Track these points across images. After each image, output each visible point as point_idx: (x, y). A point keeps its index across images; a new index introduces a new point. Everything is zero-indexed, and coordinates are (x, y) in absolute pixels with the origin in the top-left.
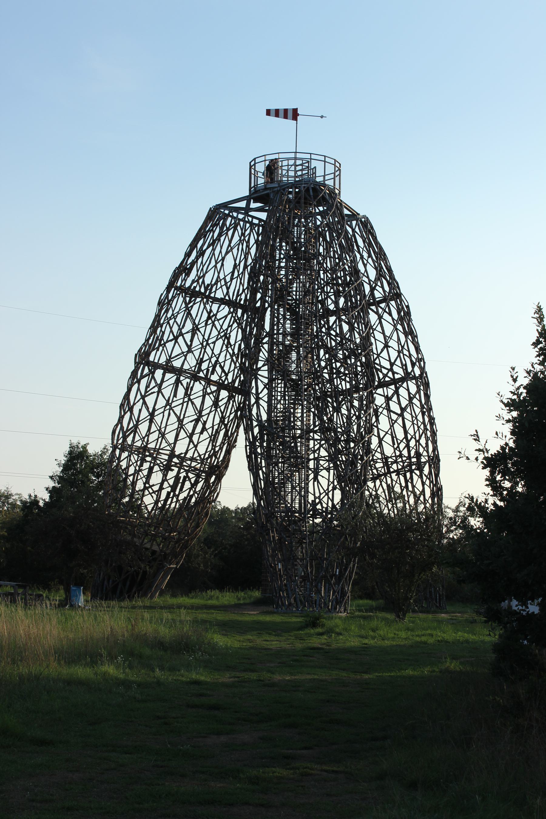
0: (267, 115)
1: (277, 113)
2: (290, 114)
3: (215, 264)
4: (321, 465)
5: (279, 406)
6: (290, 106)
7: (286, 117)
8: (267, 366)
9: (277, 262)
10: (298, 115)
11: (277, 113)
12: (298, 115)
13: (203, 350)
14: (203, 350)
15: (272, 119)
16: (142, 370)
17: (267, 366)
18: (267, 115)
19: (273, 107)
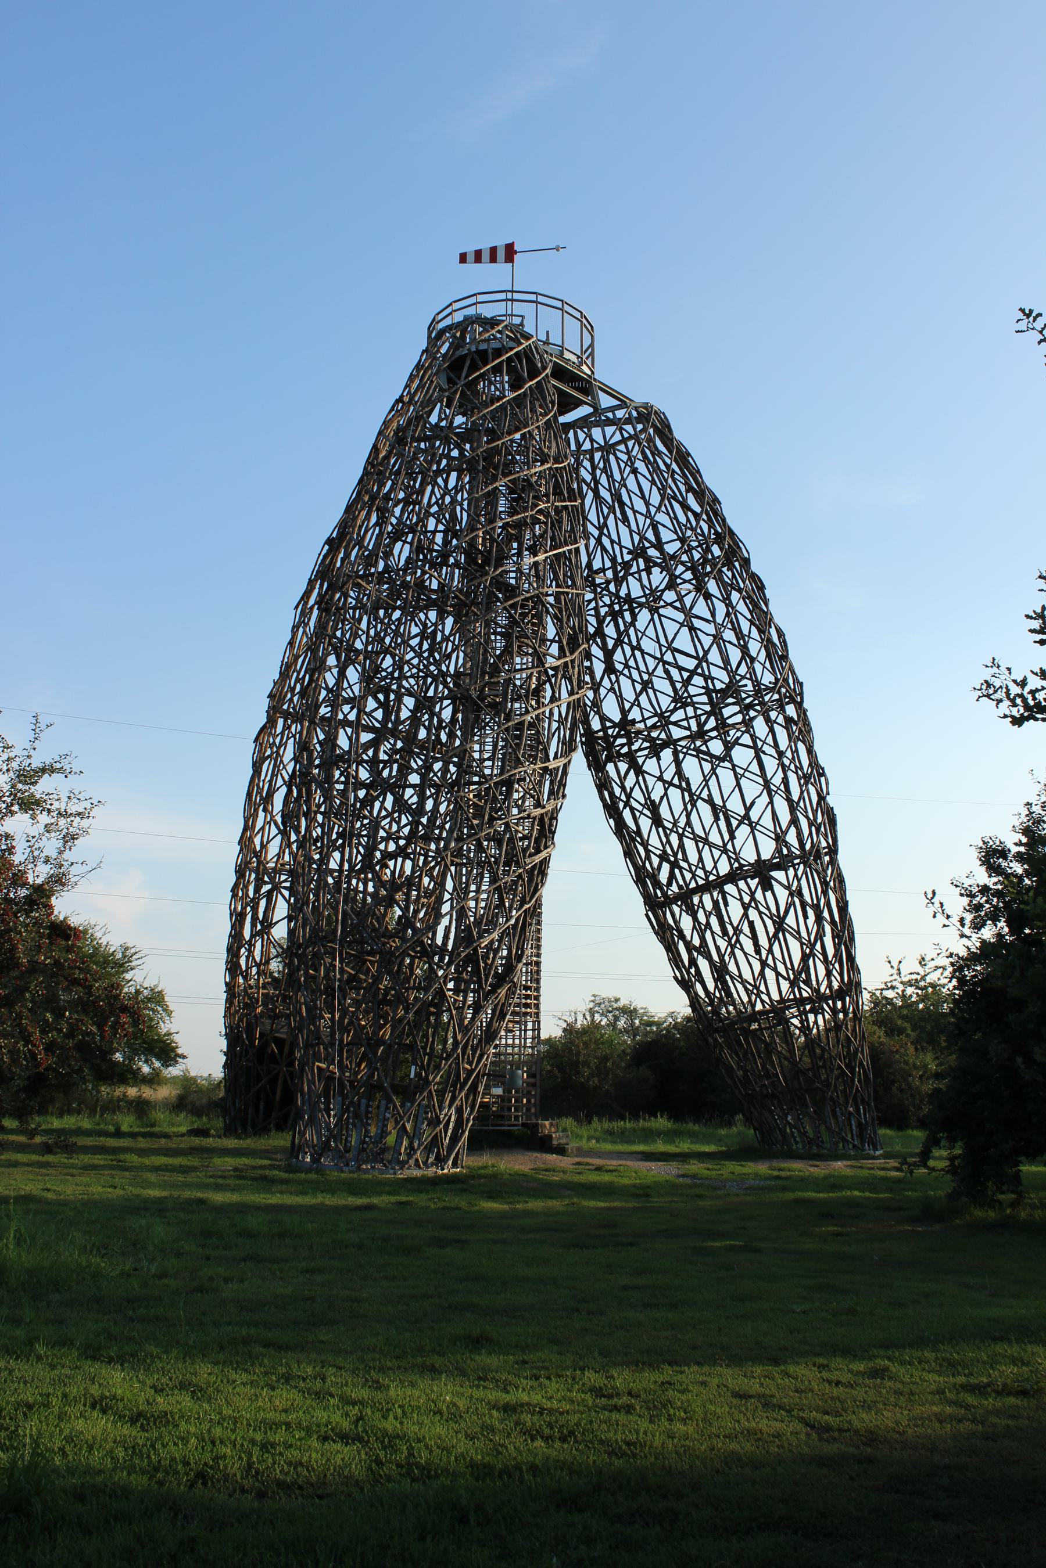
0: (461, 262)
1: (478, 256)
2: (501, 254)
3: (742, 911)
4: (675, 786)
5: (426, 880)
6: (501, 242)
7: (493, 259)
8: (698, 945)
9: (528, 1045)
10: (516, 252)
11: (478, 256)
12: (516, 252)
13: (663, 642)
14: (663, 642)
15: (471, 267)
16: (38, 1162)
17: (698, 945)
18: (461, 262)
19: (470, 249)
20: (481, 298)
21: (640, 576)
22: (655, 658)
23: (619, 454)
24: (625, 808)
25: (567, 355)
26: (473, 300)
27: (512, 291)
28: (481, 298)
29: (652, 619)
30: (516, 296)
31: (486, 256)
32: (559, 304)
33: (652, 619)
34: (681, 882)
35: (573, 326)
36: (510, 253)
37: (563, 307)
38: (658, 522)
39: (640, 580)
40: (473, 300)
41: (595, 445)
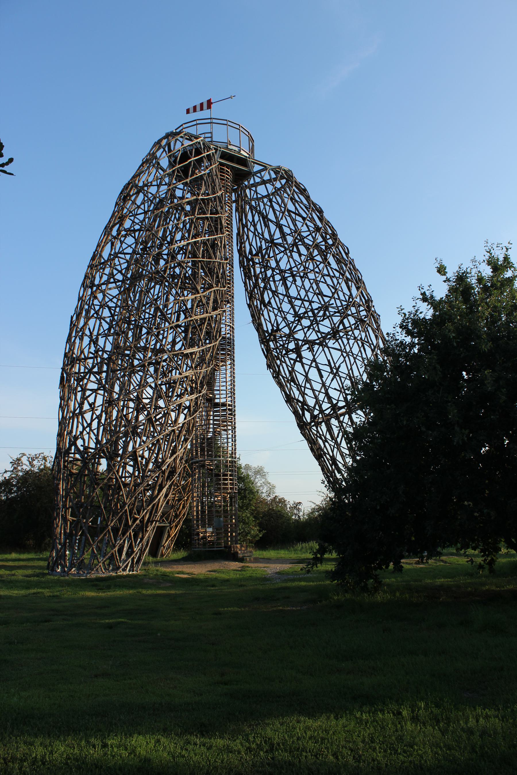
2: (205, 106)
6: (205, 100)
7: (202, 109)
10: (212, 103)
20: (198, 122)
21: (295, 263)
22: (283, 295)
23: (313, 431)
24: (113, 421)
25: (242, 152)
26: (195, 123)
27: (211, 119)
28: (198, 122)
29: (289, 261)
30: (214, 121)
31: (198, 108)
32: (238, 127)
33: (289, 261)
34: (277, 299)
35: (245, 139)
36: (209, 103)
37: (239, 128)
38: (282, 225)
39: (326, 282)
40: (195, 123)
41: (316, 311)
